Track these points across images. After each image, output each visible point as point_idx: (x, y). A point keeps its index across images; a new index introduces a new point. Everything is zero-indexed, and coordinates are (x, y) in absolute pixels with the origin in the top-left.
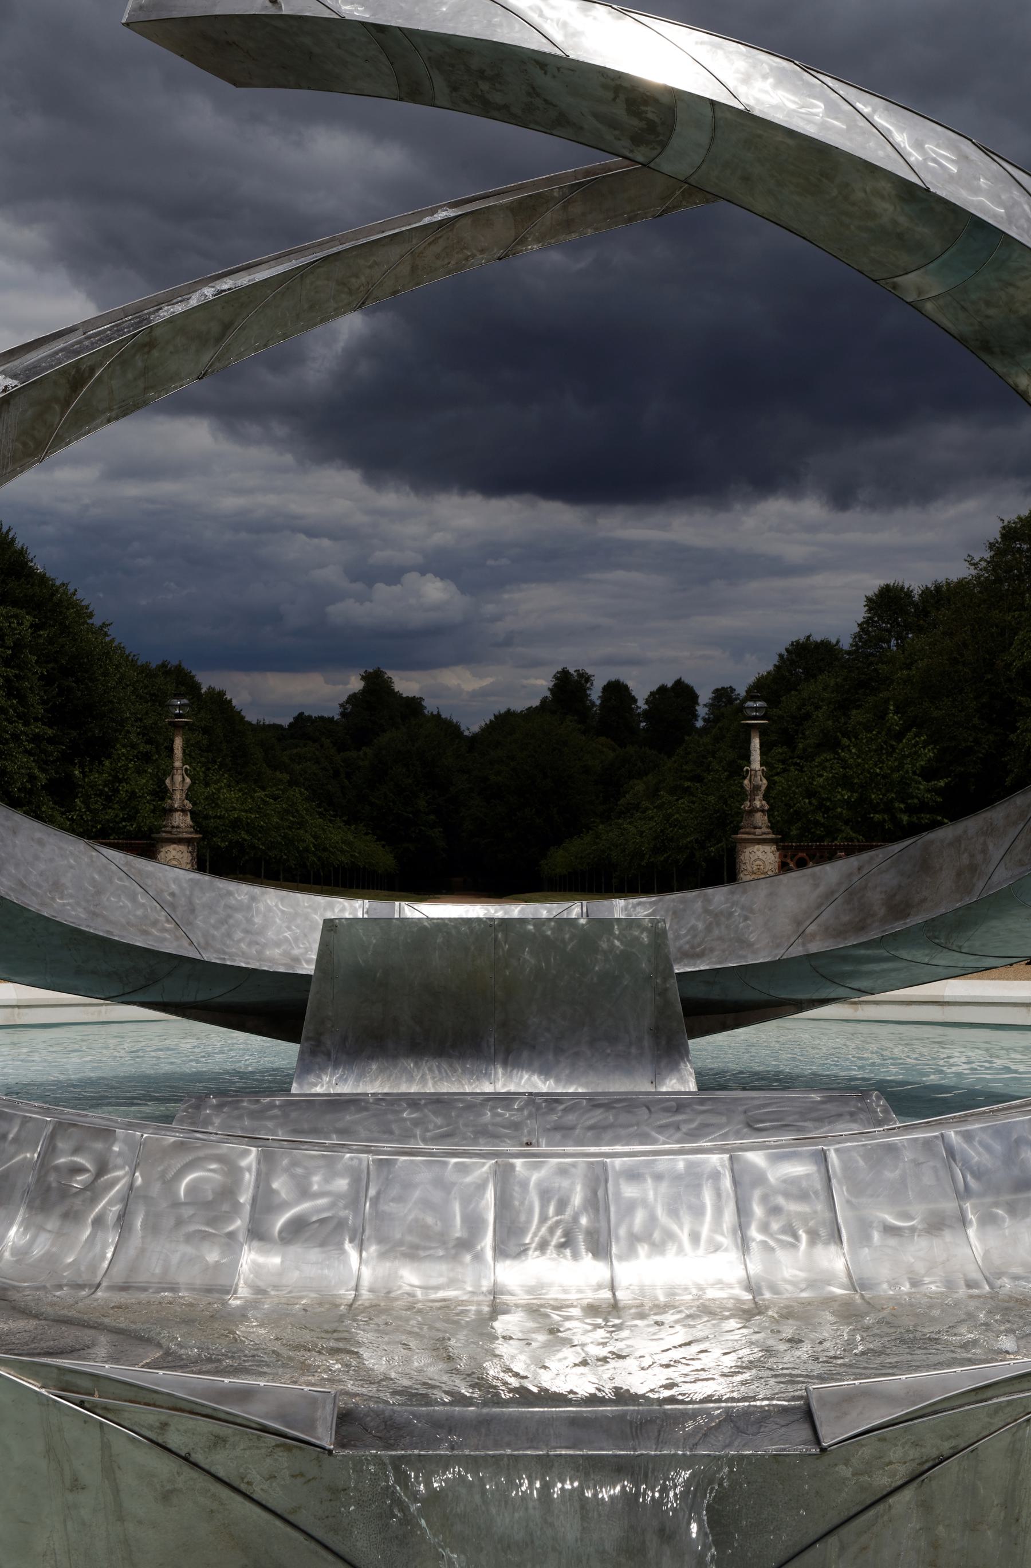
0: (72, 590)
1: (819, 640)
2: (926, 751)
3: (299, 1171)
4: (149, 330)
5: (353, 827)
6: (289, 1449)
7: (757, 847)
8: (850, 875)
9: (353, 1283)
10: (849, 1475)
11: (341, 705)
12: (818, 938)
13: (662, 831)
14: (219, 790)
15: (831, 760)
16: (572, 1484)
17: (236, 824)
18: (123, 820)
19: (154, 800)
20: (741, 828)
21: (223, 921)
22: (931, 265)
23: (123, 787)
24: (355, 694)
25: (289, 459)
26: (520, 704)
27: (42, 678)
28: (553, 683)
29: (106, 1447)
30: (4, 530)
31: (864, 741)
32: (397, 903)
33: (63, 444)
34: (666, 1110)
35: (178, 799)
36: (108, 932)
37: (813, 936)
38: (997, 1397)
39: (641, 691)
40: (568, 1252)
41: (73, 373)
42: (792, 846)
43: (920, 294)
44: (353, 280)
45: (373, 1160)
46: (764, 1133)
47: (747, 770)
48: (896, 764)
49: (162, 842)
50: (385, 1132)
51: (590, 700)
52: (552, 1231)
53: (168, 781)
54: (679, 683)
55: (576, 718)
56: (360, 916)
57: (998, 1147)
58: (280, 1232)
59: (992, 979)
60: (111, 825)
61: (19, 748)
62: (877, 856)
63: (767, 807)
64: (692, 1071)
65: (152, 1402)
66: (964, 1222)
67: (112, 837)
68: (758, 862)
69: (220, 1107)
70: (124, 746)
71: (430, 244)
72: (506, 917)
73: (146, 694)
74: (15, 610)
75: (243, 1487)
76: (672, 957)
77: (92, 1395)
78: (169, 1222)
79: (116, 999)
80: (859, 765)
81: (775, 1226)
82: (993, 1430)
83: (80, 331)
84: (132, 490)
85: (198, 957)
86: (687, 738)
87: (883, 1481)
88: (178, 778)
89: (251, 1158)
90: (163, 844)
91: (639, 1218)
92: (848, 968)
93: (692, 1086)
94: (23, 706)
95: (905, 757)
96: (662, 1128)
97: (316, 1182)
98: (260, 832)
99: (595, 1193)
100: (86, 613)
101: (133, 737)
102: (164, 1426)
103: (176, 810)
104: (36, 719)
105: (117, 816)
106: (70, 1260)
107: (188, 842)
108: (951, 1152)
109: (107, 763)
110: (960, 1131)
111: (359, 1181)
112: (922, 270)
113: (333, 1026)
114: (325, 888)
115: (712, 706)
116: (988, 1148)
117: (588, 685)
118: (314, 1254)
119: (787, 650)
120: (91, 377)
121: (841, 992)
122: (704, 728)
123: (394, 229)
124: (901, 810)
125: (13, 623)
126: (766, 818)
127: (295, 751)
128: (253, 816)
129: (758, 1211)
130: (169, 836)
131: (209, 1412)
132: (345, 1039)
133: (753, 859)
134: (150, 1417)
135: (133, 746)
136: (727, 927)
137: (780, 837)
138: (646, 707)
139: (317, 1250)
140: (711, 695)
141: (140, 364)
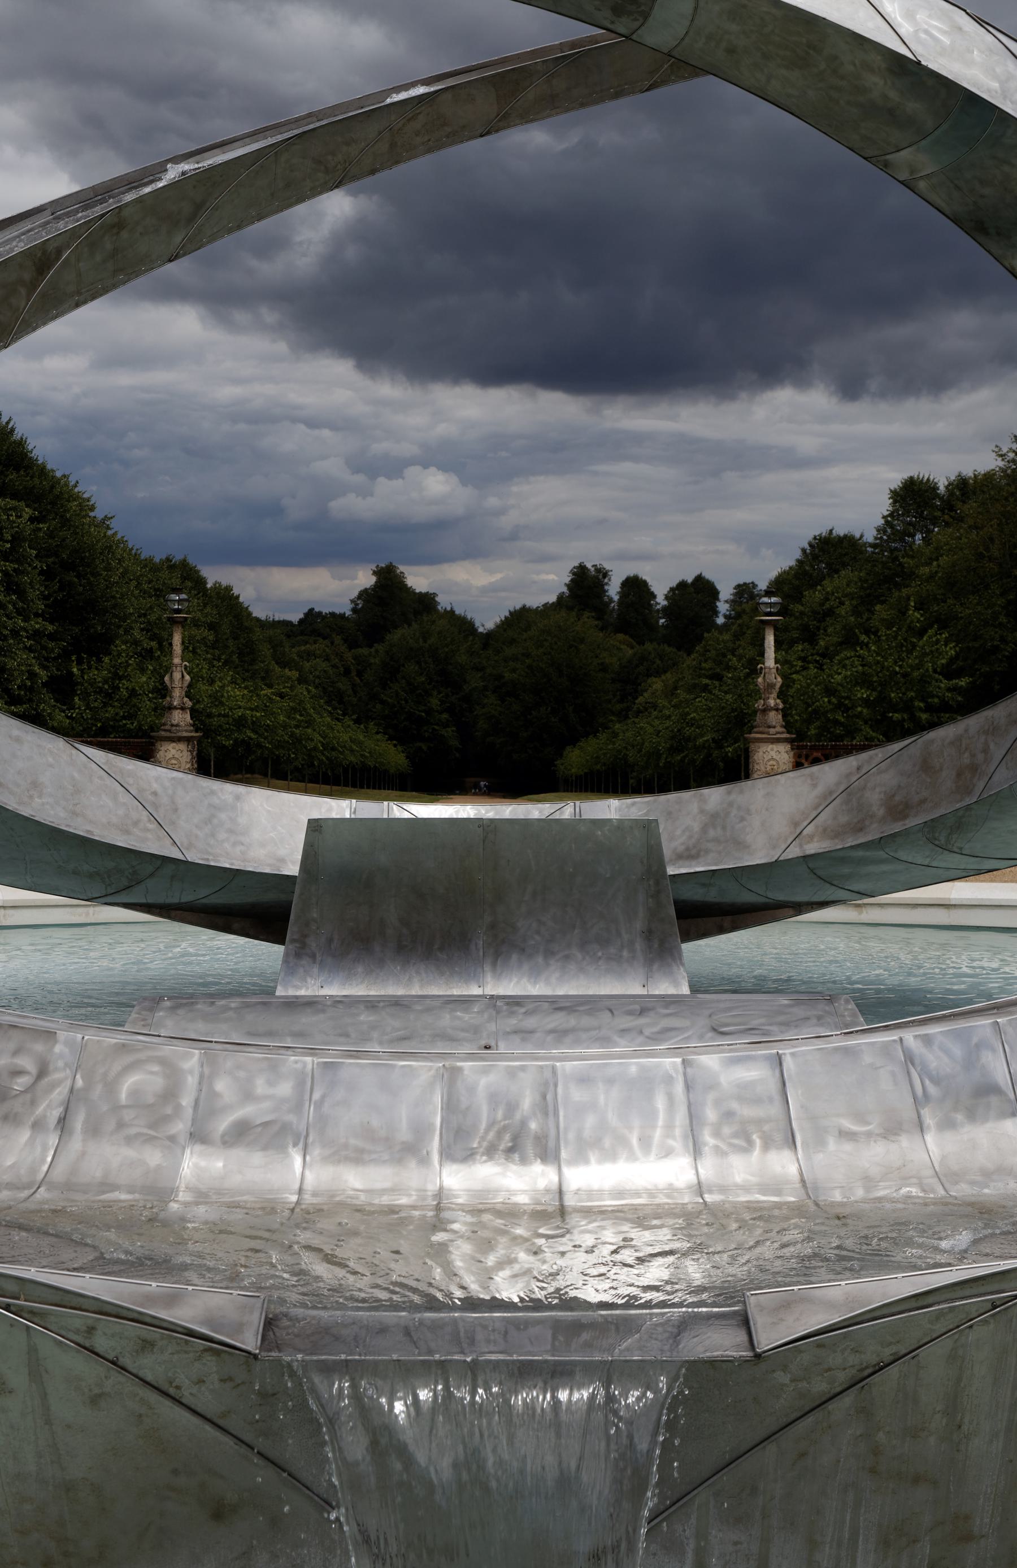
0: (72, 483)
1: (842, 535)
2: (948, 649)
3: (242, 1074)
4: (117, 210)
5: (362, 726)
6: (217, 1353)
7: (771, 746)
8: (848, 775)
9: (297, 1186)
10: (787, 1381)
11: (352, 601)
12: (815, 840)
13: (679, 730)
14: (223, 687)
15: (851, 657)
16: (487, 1389)
17: (240, 723)
18: (124, 718)
19: (155, 698)
20: (756, 727)
21: (208, 821)
22: (923, 142)
23: (124, 684)
24: (366, 589)
25: (282, 347)
26: (536, 601)
27: (42, 573)
28: (570, 579)
29: (32, 1351)
30: (4, 420)
31: (884, 638)
32: (386, 803)
33: (30, 329)
34: (630, 1013)
35: (177, 696)
36: (88, 831)
37: (811, 837)
38: (939, 1303)
39: (660, 590)
40: (516, 1156)
41: (39, 255)
42: (807, 745)
43: (912, 172)
44: (330, 158)
45: (318, 1063)
46: (728, 1037)
47: (761, 668)
48: (917, 661)
49: (161, 740)
50: (341, 1035)
51: (608, 596)
52: (500, 1134)
53: (167, 678)
54: (699, 579)
55: (593, 614)
56: (348, 816)
57: (958, 1051)
58: (223, 1136)
59: (1005, 882)
60: (111, 723)
61: (18, 644)
62: (877, 755)
63: (781, 706)
64: (685, 974)
65: (78, 1306)
66: (921, 1127)
67: (112, 736)
68: (771, 762)
69: (173, 1009)
70: (125, 643)
71: (409, 120)
72: (497, 817)
73: (151, 588)
74: (13, 502)
75: (172, 1391)
76: (666, 859)
77: (18, 1299)
78: (111, 1125)
79: (99, 900)
80: (878, 662)
81: (727, 1130)
82: (934, 1336)
83: (48, 212)
84: (125, 379)
85: (181, 857)
86: (706, 635)
87: (820, 1387)
88: (177, 676)
89: (191, 1060)
90: (163, 743)
91: (590, 1121)
92: (846, 870)
93: (685, 990)
94: (23, 602)
95: (925, 654)
96: (624, 1032)
97: (261, 1087)
98: (266, 730)
99: (544, 1097)
100: (87, 505)
101: (137, 634)
102: (91, 1330)
103: (175, 708)
104: (37, 615)
105: (117, 714)
106: (9, 1163)
107: (188, 740)
108: (909, 1058)
109: (106, 660)
110: (919, 1035)
111: (303, 1083)
112: (914, 147)
113: (318, 928)
114: (334, 788)
115: (733, 603)
116: (947, 1052)
117: (606, 580)
118: (257, 1158)
119: (810, 545)
120: (58, 259)
121: (841, 894)
122: (725, 625)
123: (374, 104)
124: (920, 709)
125: (12, 515)
126: (780, 717)
127: (303, 648)
128: (258, 714)
129: (711, 1114)
130: (168, 734)
131: (135, 1316)
132: (330, 941)
133: (766, 760)
134: (77, 1319)
135: (136, 643)
136: (724, 828)
137: (794, 736)
138: (665, 603)
139: (260, 1154)
140: (733, 591)
141: (109, 246)
